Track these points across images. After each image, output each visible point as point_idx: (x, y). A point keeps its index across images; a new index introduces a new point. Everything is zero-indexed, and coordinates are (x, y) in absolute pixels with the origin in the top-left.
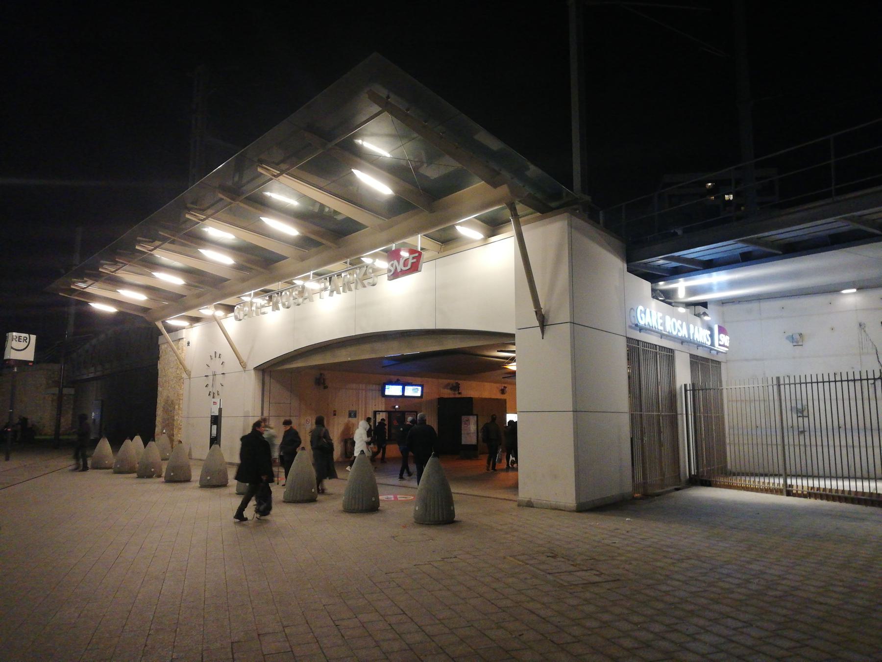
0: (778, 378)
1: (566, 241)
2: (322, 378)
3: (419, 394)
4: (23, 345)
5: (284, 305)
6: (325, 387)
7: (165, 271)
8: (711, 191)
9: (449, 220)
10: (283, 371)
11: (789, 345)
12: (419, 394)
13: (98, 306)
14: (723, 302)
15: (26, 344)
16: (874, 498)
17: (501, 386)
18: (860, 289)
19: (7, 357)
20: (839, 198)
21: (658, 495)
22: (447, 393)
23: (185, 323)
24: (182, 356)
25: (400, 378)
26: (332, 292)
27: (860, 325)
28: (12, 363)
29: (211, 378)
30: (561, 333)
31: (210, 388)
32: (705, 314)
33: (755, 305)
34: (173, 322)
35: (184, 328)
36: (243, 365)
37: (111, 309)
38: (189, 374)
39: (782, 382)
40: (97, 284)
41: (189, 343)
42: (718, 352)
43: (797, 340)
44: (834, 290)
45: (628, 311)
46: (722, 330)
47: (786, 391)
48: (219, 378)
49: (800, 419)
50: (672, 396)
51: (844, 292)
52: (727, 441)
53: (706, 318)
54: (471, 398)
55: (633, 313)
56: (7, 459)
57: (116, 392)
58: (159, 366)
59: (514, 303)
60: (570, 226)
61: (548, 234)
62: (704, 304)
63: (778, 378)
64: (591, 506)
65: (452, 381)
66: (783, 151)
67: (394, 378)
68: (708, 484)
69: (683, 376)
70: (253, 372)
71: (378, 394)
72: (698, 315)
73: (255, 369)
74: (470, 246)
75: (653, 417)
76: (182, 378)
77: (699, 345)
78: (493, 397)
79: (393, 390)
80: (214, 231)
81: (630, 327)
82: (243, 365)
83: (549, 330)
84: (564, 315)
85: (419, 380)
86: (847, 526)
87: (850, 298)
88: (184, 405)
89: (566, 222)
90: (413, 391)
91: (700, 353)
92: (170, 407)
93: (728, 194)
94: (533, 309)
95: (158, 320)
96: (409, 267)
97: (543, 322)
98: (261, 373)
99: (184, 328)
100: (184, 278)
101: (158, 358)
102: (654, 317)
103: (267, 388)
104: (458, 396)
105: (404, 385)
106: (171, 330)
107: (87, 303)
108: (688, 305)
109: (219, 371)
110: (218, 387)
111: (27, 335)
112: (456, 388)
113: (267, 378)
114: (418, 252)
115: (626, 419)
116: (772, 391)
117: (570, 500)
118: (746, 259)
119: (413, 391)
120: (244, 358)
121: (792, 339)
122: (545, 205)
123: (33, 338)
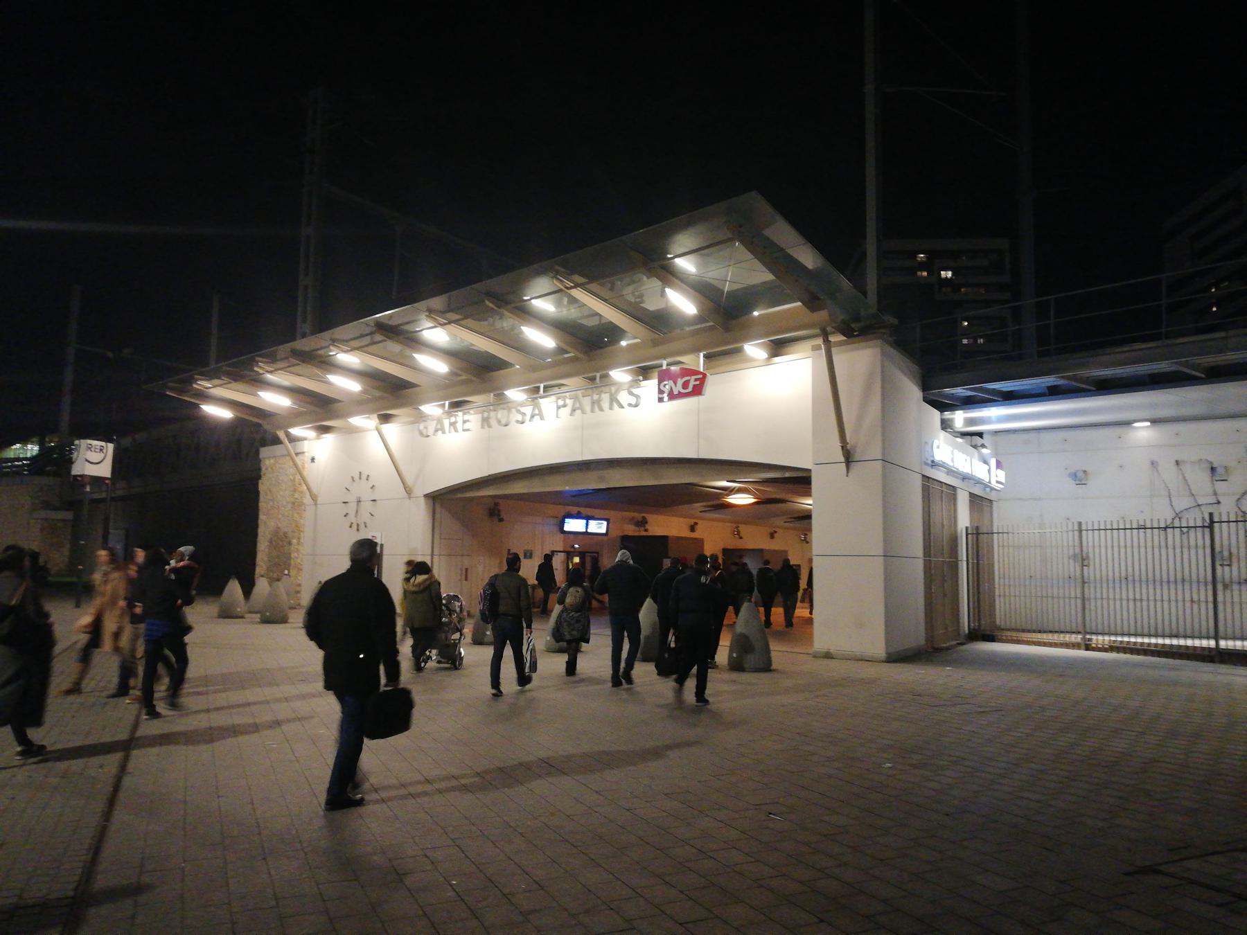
0: (1080, 524)
1: (879, 369)
2: (494, 511)
3: (603, 531)
4: (95, 457)
5: (499, 422)
6: (501, 520)
7: (342, 375)
8: (922, 266)
9: (737, 341)
10: (472, 499)
11: (1071, 484)
12: (603, 531)
13: (213, 411)
14: (997, 432)
15: (102, 455)
16: (1182, 651)
17: (692, 521)
18: (1155, 421)
19: (77, 470)
20: (1169, 342)
21: (948, 649)
22: (631, 530)
23: (311, 434)
24: (305, 473)
25: (582, 510)
26: (574, 410)
27: (1152, 463)
28: (87, 480)
29: (353, 506)
30: (869, 472)
31: (352, 518)
32: (983, 446)
33: (1033, 435)
34: (296, 431)
35: (305, 439)
36: (408, 491)
37: (225, 414)
38: (314, 498)
39: (1084, 527)
40: (234, 385)
41: (313, 460)
42: (992, 489)
43: (1080, 478)
44: (1128, 423)
45: (924, 445)
46: (999, 465)
47: (1088, 537)
48: (367, 507)
49: (1227, 568)
50: (954, 540)
51: (1136, 425)
52: (997, 593)
53: (984, 451)
54: (665, 538)
55: (928, 448)
56: (78, 606)
57: (205, 518)
58: (262, 487)
59: (810, 435)
60: (883, 354)
61: (860, 361)
62: (980, 435)
63: (1080, 524)
64: (898, 657)
65: (638, 516)
66: (869, 89)
67: (574, 510)
68: (991, 639)
69: (964, 519)
70: (422, 500)
71: (556, 529)
72: (975, 447)
73: (426, 496)
74: (749, 365)
75: (940, 563)
76: (301, 504)
77: (978, 482)
78: (683, 535)
79: (574, 525)
80: (436, 335)
81: (926, 464)
82: (408, 491)
83: (856, 468)
84: (875, 451)
85: (607, 513)
86: (1173, 674)
87: (1143, 432)
88: (307, 535)
89: (878, 350)
90: (599, 527)
91: (977, 491)
92: (282, 543)
93: (945, 270)
94: (838, 445)
95: (281, 428)
96: (690, 389)
97: (849, 458)
98: (431, 502)
99: (305, 439)
100: (361, 383)
101: (259, 477)
102: (948, 453)
103: (437, 516)
104: (644, 534)
105: (588, 518)
106: (293, 439)
107: (197, 406)
108: (964, 435)
109: (367, 495)
110: (364, 516)
111: (103, 444)
112: (642, 523)
113: (438, 508)
114: (698, 373)
115: (920, 564)
116: (1072, 538)
117: (880, 650)
118: (1053, 393)
119: (599, 527)
120: (409, 481)
121: (1074, 476)
122: (855, 328)
123: (111, 446)
